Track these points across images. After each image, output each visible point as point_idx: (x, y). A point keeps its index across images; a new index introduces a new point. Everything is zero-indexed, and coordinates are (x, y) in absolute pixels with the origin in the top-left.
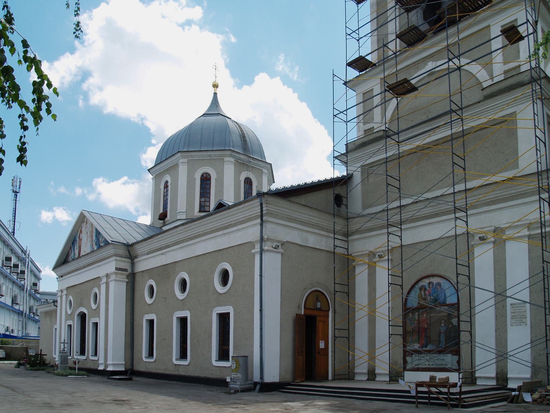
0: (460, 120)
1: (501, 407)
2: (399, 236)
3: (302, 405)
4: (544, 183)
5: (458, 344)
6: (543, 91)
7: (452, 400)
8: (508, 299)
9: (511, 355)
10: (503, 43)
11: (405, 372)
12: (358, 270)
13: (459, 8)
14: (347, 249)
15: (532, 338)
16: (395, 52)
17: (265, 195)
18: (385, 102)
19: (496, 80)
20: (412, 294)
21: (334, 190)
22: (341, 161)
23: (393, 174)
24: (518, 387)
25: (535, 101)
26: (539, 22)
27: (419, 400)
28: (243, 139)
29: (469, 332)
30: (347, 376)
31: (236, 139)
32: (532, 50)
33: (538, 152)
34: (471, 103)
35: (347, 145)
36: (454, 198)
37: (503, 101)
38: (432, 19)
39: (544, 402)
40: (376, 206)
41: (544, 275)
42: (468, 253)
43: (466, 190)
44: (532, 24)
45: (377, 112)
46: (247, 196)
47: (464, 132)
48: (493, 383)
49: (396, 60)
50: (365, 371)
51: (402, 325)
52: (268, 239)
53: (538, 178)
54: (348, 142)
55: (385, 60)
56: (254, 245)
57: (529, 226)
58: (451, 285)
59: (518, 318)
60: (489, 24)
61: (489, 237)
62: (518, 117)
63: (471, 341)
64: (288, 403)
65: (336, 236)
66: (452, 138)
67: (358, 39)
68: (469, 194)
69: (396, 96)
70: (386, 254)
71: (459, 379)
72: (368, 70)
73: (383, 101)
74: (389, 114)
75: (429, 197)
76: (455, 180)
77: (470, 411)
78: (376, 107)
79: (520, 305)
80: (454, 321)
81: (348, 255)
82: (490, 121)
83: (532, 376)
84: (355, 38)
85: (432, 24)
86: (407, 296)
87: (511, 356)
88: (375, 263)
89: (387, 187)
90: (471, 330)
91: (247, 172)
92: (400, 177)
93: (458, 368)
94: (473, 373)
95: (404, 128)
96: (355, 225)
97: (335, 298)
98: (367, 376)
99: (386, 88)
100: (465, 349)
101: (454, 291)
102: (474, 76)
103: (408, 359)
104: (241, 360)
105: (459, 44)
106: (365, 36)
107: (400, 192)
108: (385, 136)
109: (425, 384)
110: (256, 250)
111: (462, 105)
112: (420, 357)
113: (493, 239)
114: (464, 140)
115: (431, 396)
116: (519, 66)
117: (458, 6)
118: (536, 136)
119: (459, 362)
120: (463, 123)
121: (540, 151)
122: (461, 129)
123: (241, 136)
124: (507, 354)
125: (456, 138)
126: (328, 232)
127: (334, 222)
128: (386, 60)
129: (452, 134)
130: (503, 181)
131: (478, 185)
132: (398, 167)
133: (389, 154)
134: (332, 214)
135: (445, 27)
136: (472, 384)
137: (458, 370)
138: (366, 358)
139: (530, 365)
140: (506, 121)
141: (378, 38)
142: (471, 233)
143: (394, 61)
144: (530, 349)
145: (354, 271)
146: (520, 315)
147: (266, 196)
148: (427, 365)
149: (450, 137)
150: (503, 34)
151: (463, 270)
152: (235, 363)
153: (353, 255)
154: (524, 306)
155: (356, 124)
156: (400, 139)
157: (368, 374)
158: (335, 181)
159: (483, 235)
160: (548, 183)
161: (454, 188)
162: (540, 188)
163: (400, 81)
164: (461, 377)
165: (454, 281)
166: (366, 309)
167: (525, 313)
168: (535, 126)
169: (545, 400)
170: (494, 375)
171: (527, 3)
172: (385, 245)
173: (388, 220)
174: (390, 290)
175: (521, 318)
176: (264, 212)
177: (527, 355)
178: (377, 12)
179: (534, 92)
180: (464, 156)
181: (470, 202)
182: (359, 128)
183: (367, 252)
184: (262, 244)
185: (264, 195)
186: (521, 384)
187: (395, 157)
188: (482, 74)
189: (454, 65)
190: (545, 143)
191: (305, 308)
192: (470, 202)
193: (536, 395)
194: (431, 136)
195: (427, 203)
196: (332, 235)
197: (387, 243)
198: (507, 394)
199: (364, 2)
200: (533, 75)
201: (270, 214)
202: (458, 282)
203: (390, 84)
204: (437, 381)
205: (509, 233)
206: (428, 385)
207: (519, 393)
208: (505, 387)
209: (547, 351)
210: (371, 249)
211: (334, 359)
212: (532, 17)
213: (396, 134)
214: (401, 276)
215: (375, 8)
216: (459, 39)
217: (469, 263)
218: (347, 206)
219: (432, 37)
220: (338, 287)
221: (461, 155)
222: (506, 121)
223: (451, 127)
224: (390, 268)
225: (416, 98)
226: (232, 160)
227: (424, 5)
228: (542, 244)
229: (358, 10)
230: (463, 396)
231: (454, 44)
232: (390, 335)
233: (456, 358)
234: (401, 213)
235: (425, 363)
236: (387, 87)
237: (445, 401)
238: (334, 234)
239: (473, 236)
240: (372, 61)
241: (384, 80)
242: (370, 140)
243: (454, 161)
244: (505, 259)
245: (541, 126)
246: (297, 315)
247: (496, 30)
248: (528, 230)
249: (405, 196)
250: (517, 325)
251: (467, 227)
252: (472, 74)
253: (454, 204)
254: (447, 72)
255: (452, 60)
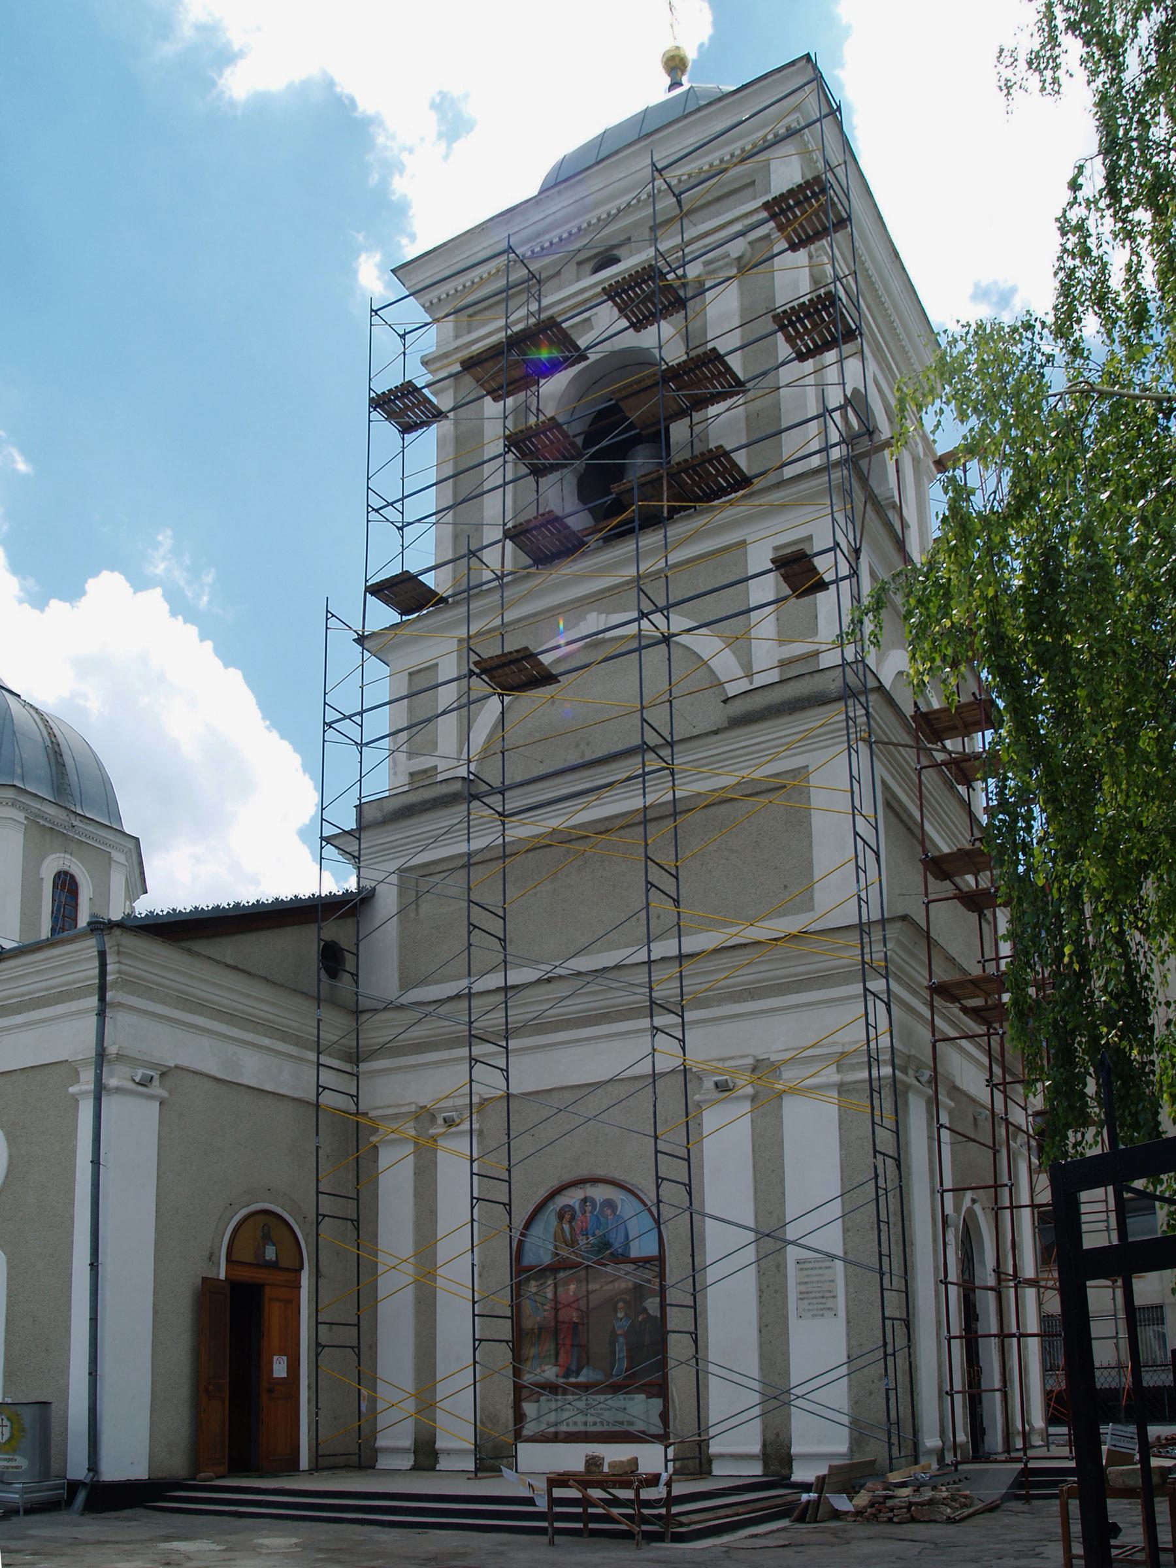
0: (667, 772)
1: (776, 1535)
2: (502, 1070)
3: (218, 1548)
4: (877, 952)
5: (662, 1365)
6: (872, 723)
7: (645, 1520)
8: (790, 1248)
9: (800, 1394)
10: (778, 591)
11: (519, 1445)
12: (385, 1158)
13: (670, 486)
14: (356, 1097)
15: (850, 1348)
16: (499, 574)
17: (115, 928)
18: (470, 703)
19: (759, 681)
20: (538, 1229)
21: (320, 928)
22: (341, 852)
23: (486, 900)
24: (818, 1478)
25: (855, 746)
26: (862, 548)
27: (557, 1525)
28: (53, 760)
29: (691, 1333)
30: (356, 1458)
31: (34, 755)
32: (846, 620)
33: (862, 874)
34: (695, 732)
35: (359, 808)
36: (650, 977)
37: (770, 737)
38: (598, 502)
39: (882, 1514)
40: (437, 982)
41: (877, 1187)
42: (687, 1122)
43: (681, 958)
44: (847, 554)
45: (448, 727)
46: (60, 924)
47: (678, 805)
48: (755, 1470)
49: (502, 597)
50: (408, 1443)
51: (509, 1315)
52: (120, 1057)
53: (862, 939)
54: (363, 800)
55: (472, 592)
56: (77, 1073)
57: (841, 1061)
58: (641, 1207)
59: (816, 1298)
60: (742, 538)
61: (740, 1083)
62: (814, 779)
63: (697, 1359)
64: (176, 1545)
65: (324, 1059)
66: (645, 818)
67: (400, 525)
68: (689, 967)
69: (500, 691)
70: (465, 1116)
71: (667, 1461)
72: (425, 612)
73: (464, 700)
74: (479, 736)
75: (583, 970)
76: (651, 927)
77: (695, 1549)
78: (444, 713)
79: (820, 1264)
80: (652, 1305)
81: (358, 1113)
82: (744, 783)
83: (851, 1449)
84: (392, 523)
85: (602, 514)
86: (522, 1234)
87: (798, 1397)
88: (436, 1141)
89: (470, 933)
90: (696, 1328)
91: (62, 855)
92: (505, 909)
93: (662, 1432)
94: (702, 1445)
95: (519, 779)
96: (378, 1031)
97: (318, 1235)
98: (412, 1457)
99: (473, 667)
100: (680, 1379)
101: (649, 1223)
102: (706, 663)
103: (529, 1408)
104: (28, 1415)
105: (667, 577)
106: (419, 520)
107: (505, 949)
108: (466, 795)
109: (575, 1481)
110: (84, 1088)
111: (671, 734)
112: (560, 1404)
113: (749, 1090)
114: (676, 827)
115: (590, 1510)
116: (816, 654)
117: (668, 482)
118: (856, 834)
119: (664, 1416)
120: (674, 780)
121: (865, 872)
122: (669, 797)
123: (50, 751)
124: (788, 1391)
125: (656, 819)
126: (301, 1047)
127: (319, 1020)
128: (476, 591)
129: (645, 808)
130: (775, 940)
131: (712, 947)
132: (501, 882)
133: (477, 844)
134: (314, 997)
135: (634, 527)
136: (701, 1473)
137: (663, 1438)
138: (410, 1406)
139: (845, 1420)
140: (785, 787)
141: (455, 530)
142: (694, 1070)
143: (496, 597)
144: (846, 1378)
145: (376, 1161)
146: (819, 1289)
147: (117, 932)
148: (579, 1424)
149: (642, 815)
150: (778, 568)
151: (673, 1169)
152: (8, 1423)
153: (372, 1114)
154: (830, 1267)
155: (387, 753)
156: (506, 807)
157: (415, 1452)
158: (322, 904)
159: (725, 1077)
160: (886, 953)
161: (649, 950)
162: (866, 966)
163: (510, 653)
164: (670, 1456)
165: (650, 1196)
166: (409, 1268)
167: (832, 1284)
168: (854, 807)
169: (884, 1510)
170: (756, 1448)
171: (834, 502)
172: (462, 1091)
173: (471, 1023)
174: (475, 1217)
175: (823, 1297)
176: (109, 978)
177: (838, 1395)
178: (456, 460)
179: (851, 723)
180: (677, 867)
181: (694, 988)
182: (395, 764)
183: (413, 1108)
184: (101, 1071)
185: (112, 928)
186: (824, 1471)
187: (495, 854)
188: (725, 664)
189: (655, 629)
190: (877, 854)
191: (229, 1260)
192: (694, 988)
193: (862, 1499)
194: (592, 807)
195: (578, 983)
196: (312, 1056)
197: (468, 1085)
198: (790, 1498)
199: (420, 431)
200: (848, 681)
201: (127, 983)
202: (659, 1201)
203: (485, 656)
204: (606, 1469)
205: (790, 1075)
206: (583, 1482)
207: (820, 1497)
208: (784, 1481)
209: (887, 1384)
210: (425, 1100)
211: (314, 1410)
212: (846, 537)
213: (495, 793)
214: (507, 1179)
215: (450, 449)
216: (667, 565)
217: (689, 1150)
218: (355, 976)
219: (598, 549)
220: (327, 1205)
221: (669, 864)
222: (785, 787)
223: (644, 788)
224: (475, 1156)
225: (553, 703)
226: (20, 816)
227: (580, 464)
228: (873, 1108)
229: (403, 447)
230: (675, 1510)
231: (655, 575)
232: (477, 1343)
233: (657, 1403)
234: (506, 1007)
235: (574, 1419)
236: (475, 663)
237: (627, 1525)
238: (319, 1053)
239: (700, 1078)
240: (437, 590)
241: (467, 645)
242: (425, 802)
243: (650, 879)
244: (782, 1141)
245: (868, 810)
246: (205, 1279)
247: (760, 557)
248: (838, 1071)
249: (519, 961)
250: (814, 1316)
251: (684, 1055)
252: (699, 657)
253: (650, 992)
254: (635, 645)
255: (650, 617)
